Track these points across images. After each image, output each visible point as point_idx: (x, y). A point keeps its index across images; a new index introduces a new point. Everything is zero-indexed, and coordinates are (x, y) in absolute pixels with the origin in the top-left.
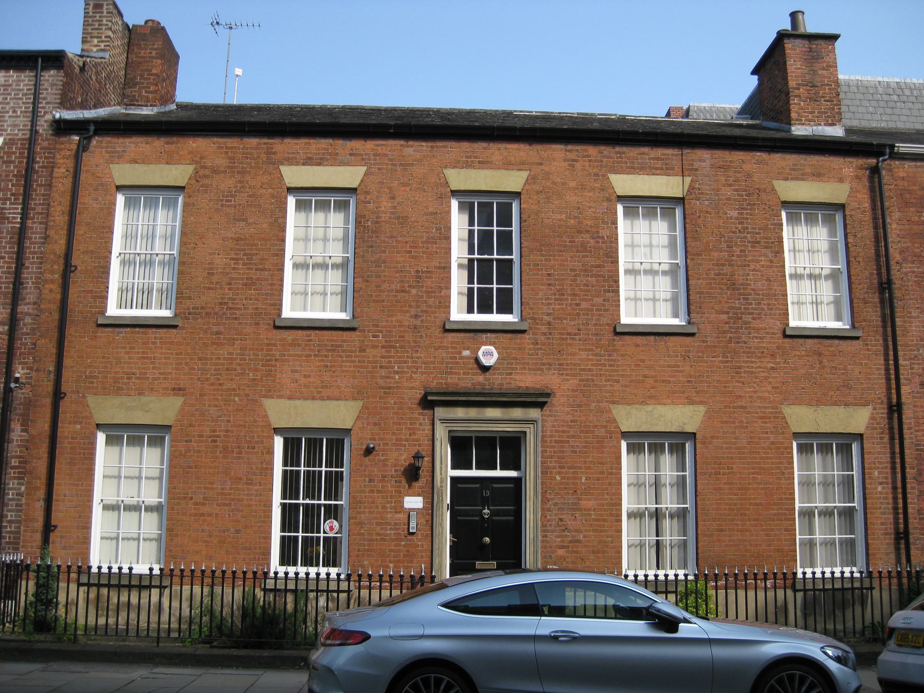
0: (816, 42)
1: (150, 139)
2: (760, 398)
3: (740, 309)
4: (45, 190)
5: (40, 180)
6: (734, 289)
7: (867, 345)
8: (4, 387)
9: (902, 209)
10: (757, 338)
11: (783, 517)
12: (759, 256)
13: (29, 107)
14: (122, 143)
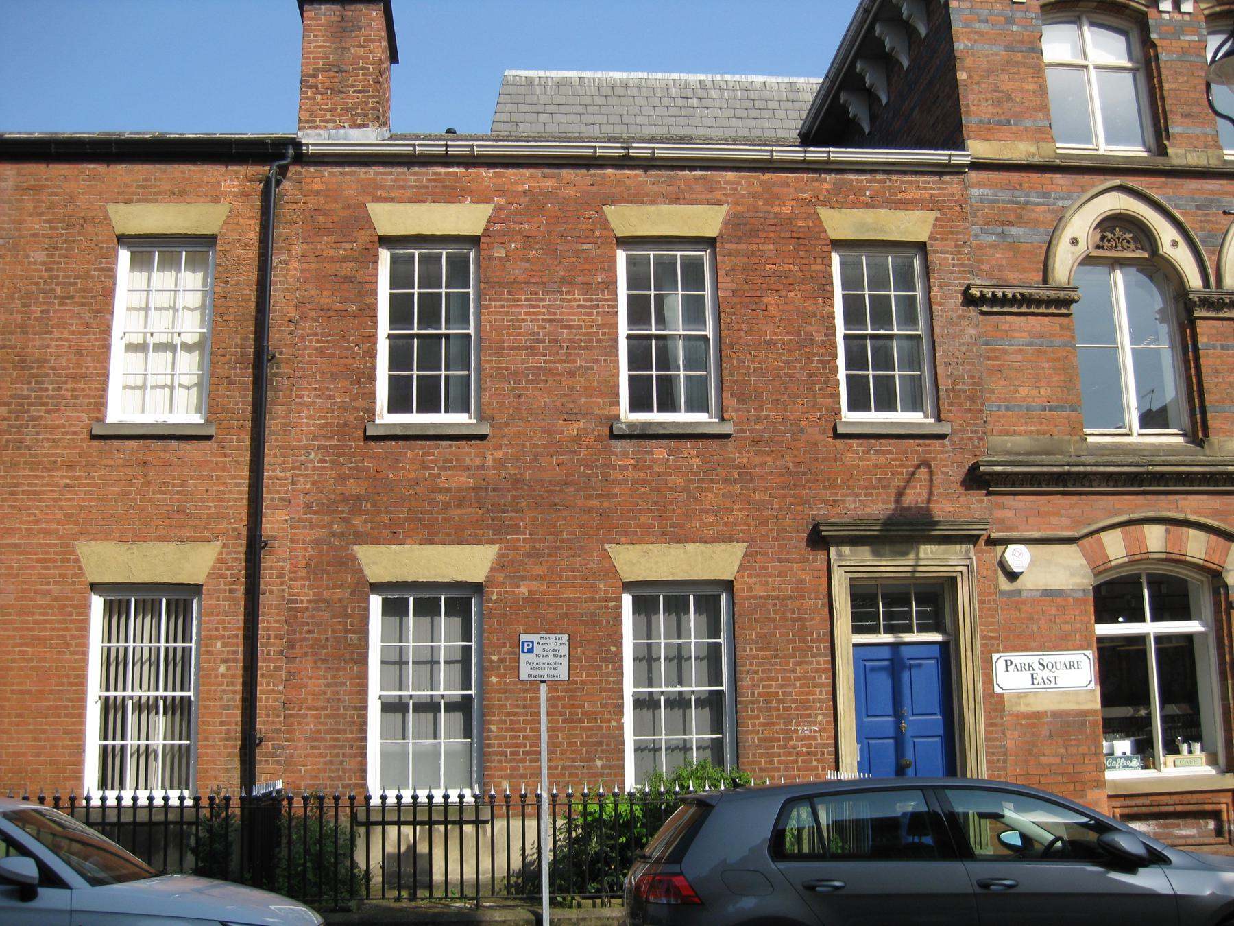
0: (353, 7)
2: (41, 530)
3: (29, 397)
6: (23, 369)
7: (224, 448)
9: (309, 240)
10: (48, 440)
11: (63, 712)
12: (70, 318)
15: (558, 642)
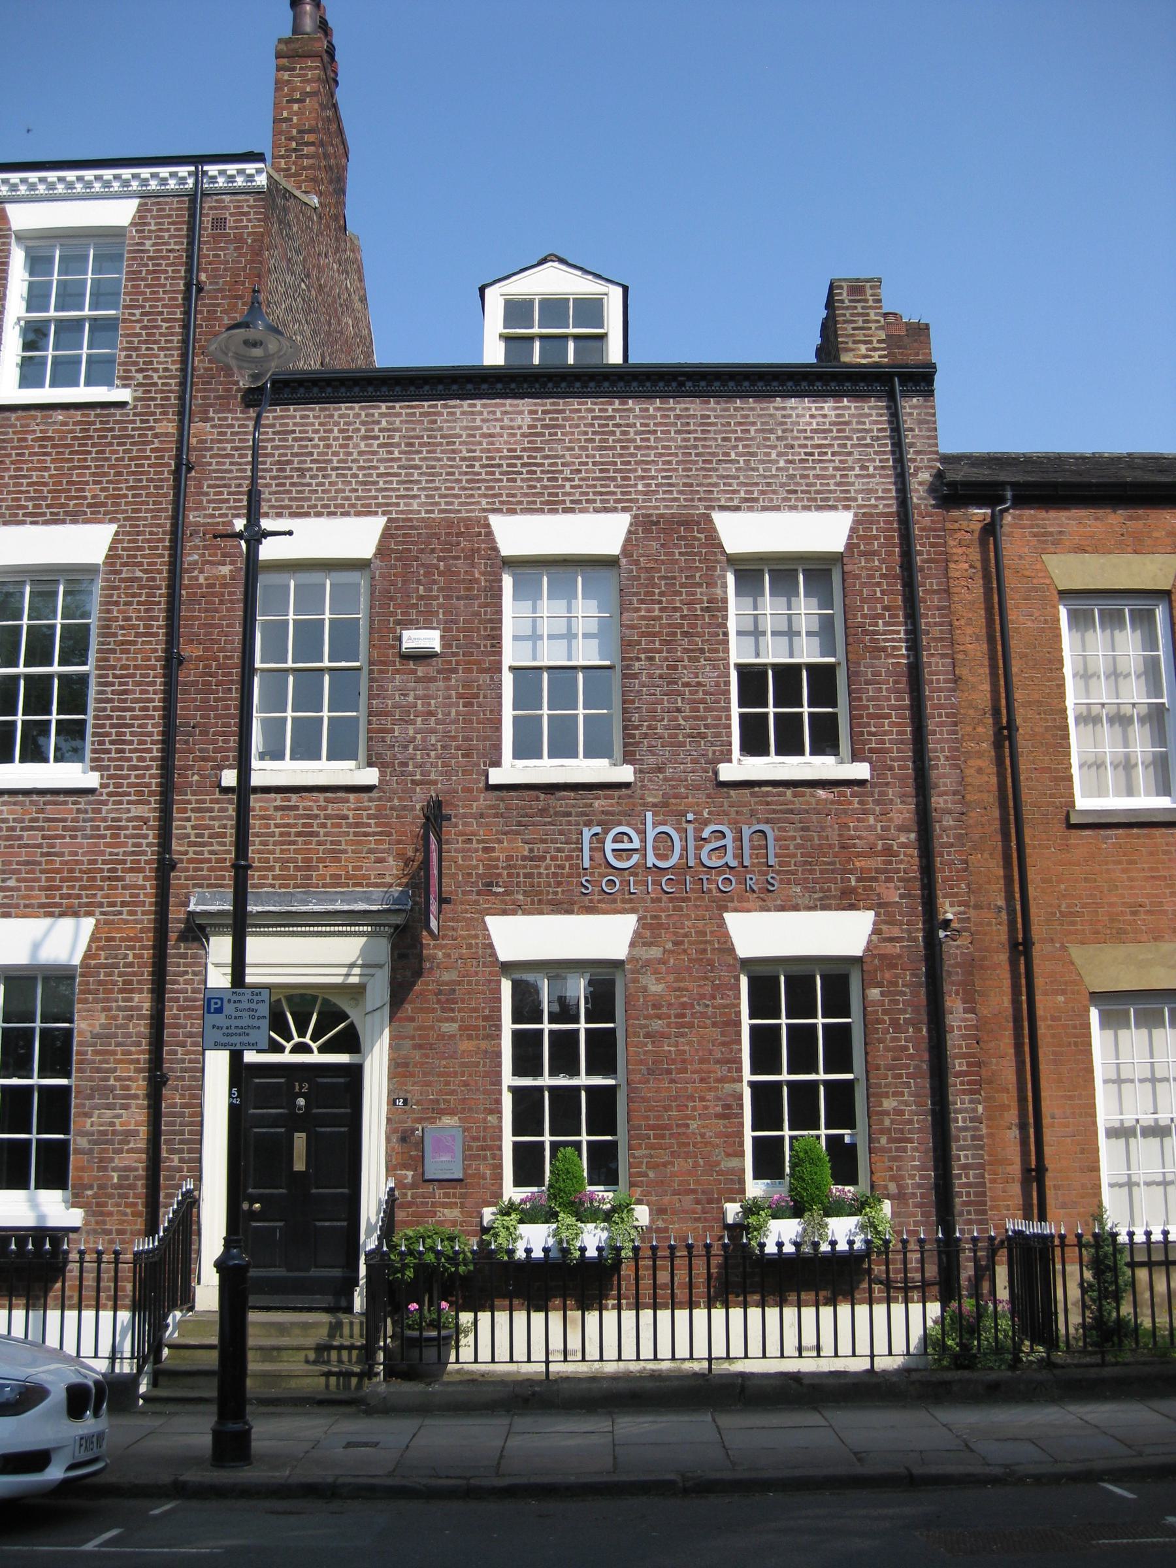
1: (1100, 513)
4: (940, 600)
5: (928, 583)
8: (924, 937)
13: (887, 460)
14: (1055, 519)
15: (256, 998)
